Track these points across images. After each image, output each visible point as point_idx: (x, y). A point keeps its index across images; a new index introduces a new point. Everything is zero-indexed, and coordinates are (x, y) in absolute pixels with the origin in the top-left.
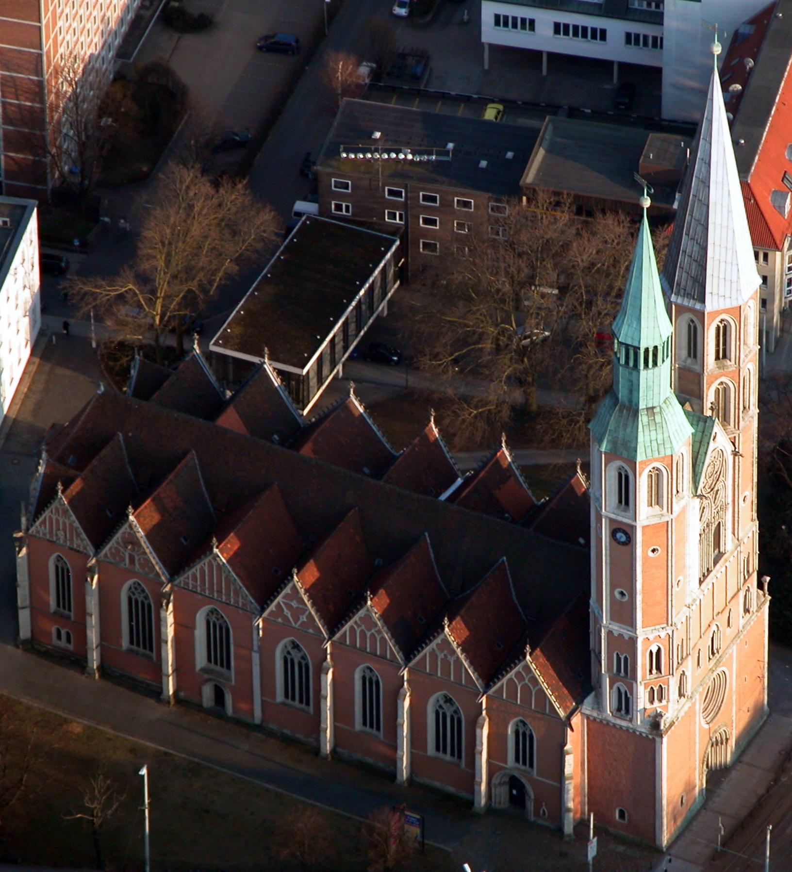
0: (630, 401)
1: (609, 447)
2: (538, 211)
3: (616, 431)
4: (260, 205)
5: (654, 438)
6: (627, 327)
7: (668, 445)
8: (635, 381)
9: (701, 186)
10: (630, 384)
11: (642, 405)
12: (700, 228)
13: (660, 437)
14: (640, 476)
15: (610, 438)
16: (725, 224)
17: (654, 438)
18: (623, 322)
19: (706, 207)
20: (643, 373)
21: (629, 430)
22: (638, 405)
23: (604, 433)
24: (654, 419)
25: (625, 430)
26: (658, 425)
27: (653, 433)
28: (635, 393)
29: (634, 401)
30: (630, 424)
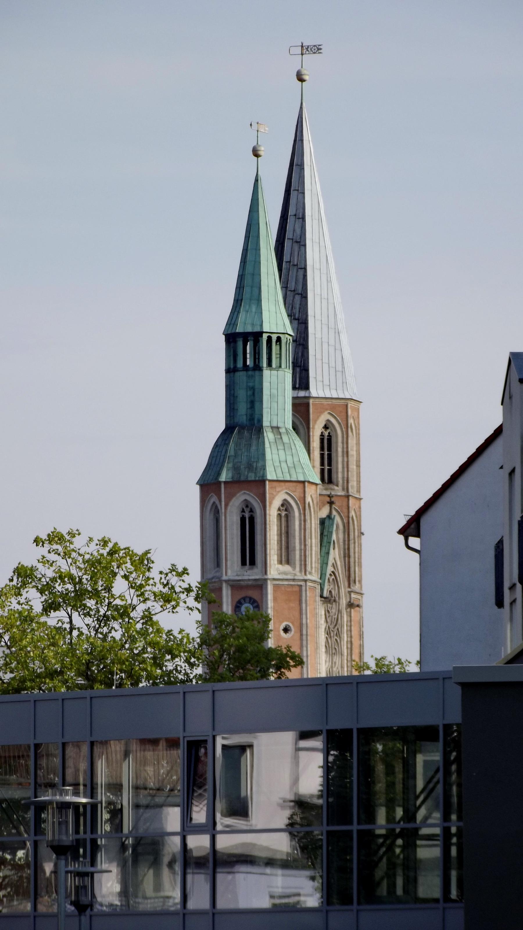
0: (251, 418)
1: (230, 475)
2: (151, 630)
3: (236, 456)
4: (105, 747)
5: (283, 458)
6: (244, 313)
7: (299, 470)
8: (257, 386)
9: (296, 247)
10: (250, 393)
11: (266, 423)
12: (298, 298)
13: (289, 459)
14: (270, 506)
15: (231, 465)
16: (325, 295)
17: (283, 458)
18: (241, 305)
19: (302, 271)
20: (266, 373)
21: (254, 448)
22: (260, 421)
23: (224, 462)
24: (281, 438)
25: (248, 450)
26: (286, 445)
27: (282, 452)
28: (257, 405)
29: (256, 417)
30: (254, 442)
